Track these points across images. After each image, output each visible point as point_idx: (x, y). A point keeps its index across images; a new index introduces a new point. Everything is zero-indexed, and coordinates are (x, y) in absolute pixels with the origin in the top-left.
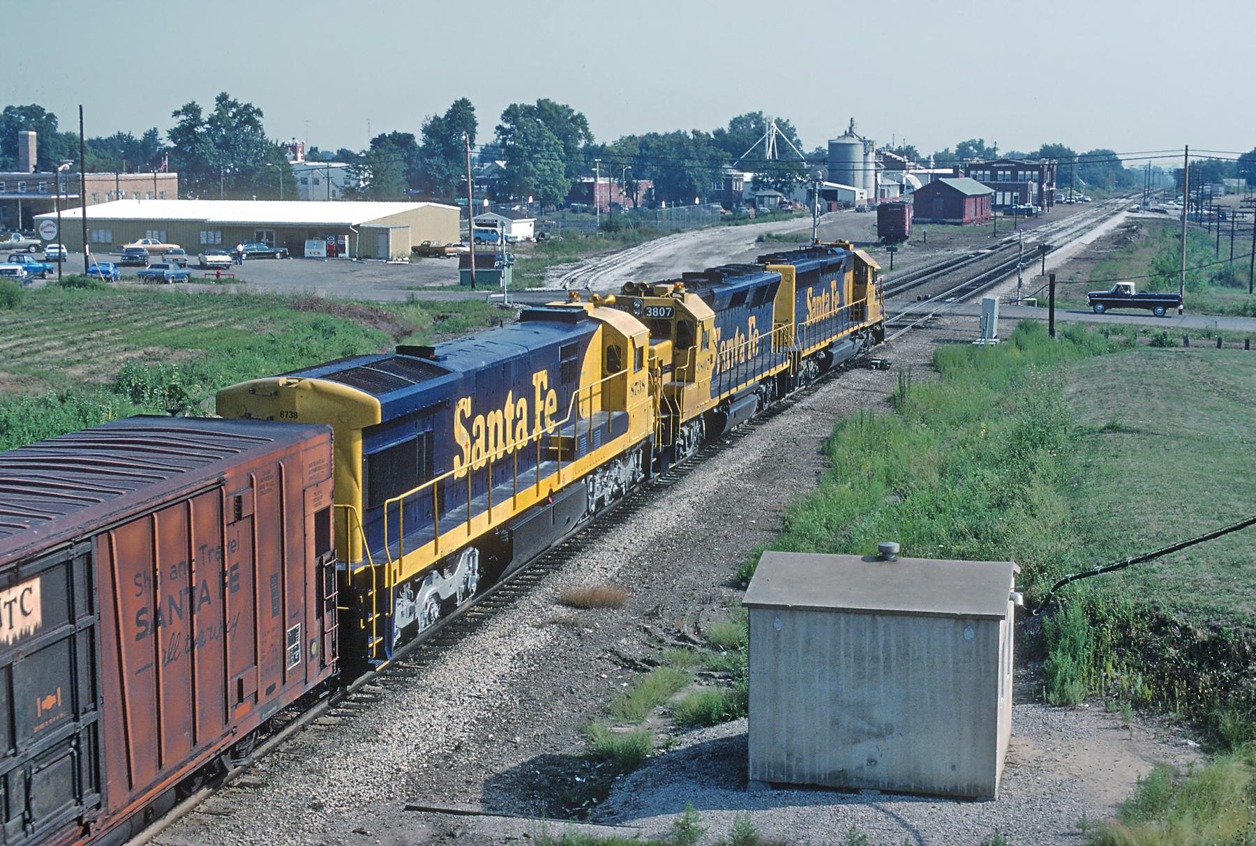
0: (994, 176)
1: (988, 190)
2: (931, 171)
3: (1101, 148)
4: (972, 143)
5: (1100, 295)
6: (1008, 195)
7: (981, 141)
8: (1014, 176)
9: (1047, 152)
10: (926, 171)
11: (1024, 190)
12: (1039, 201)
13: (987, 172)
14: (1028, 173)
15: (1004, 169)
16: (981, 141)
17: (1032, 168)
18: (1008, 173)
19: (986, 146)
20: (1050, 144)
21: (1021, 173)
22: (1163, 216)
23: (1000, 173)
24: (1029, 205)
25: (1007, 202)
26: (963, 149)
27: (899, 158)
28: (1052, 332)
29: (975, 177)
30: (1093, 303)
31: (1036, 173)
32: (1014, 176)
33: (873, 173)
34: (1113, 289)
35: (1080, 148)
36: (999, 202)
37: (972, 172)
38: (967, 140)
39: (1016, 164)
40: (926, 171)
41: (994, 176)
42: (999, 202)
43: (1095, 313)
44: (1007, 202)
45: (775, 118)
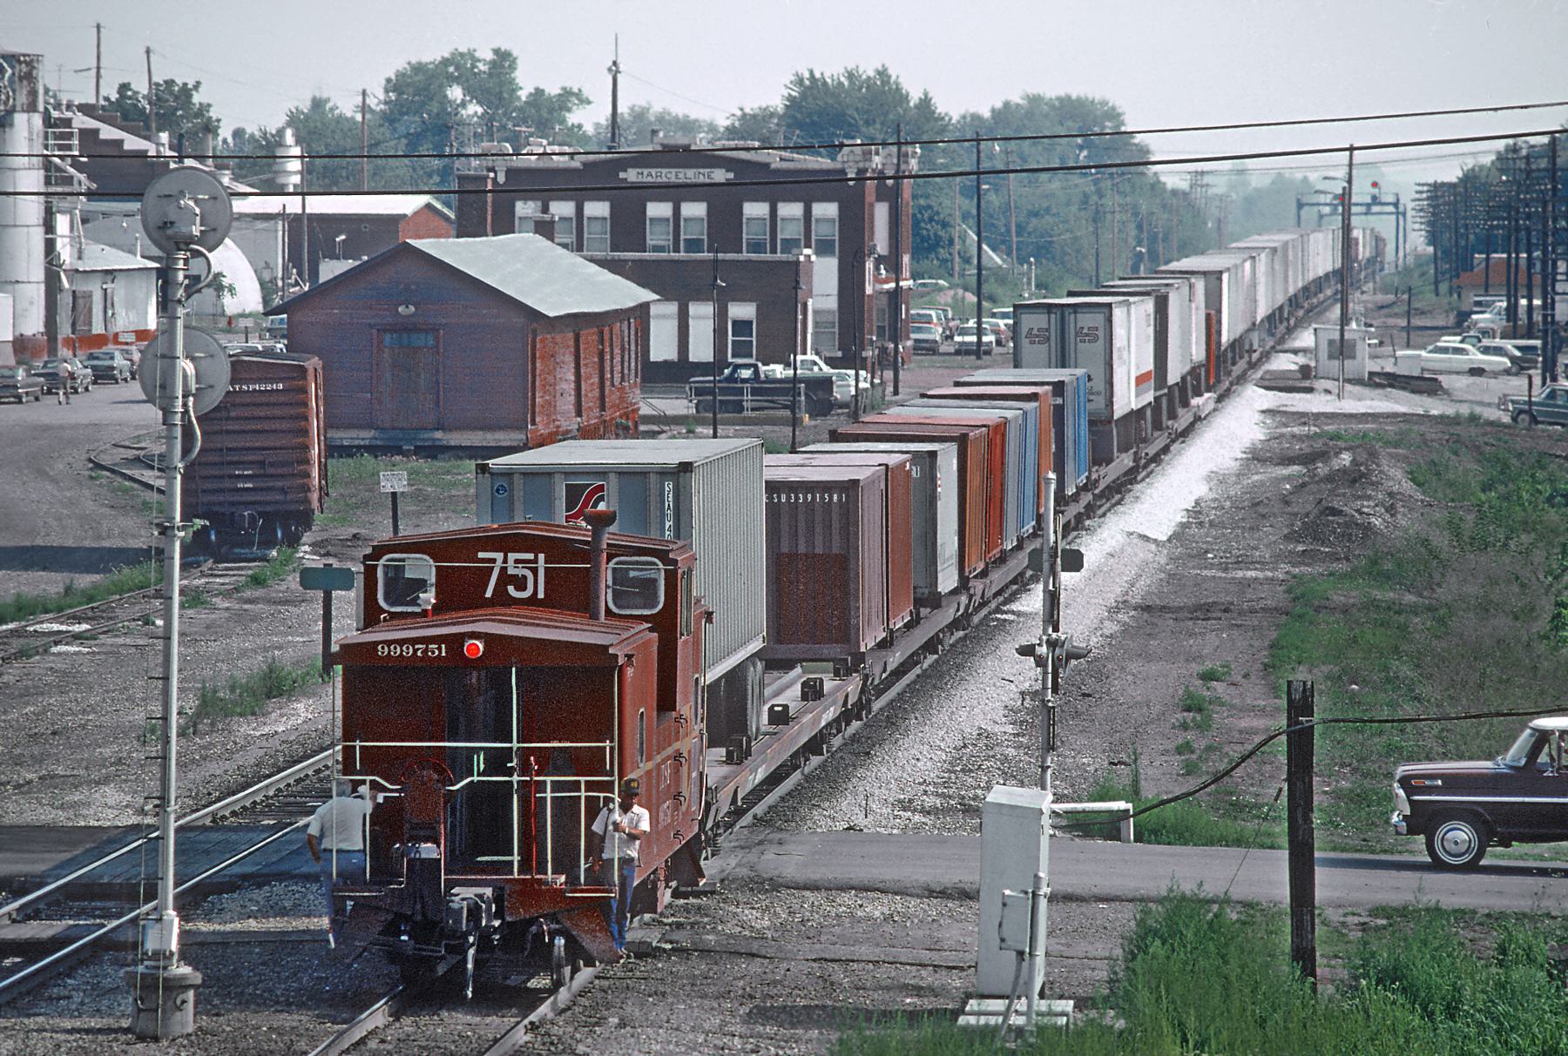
0: (628, 227)
1: (624, 293)
2: (293, 205)
3: (1052, 88)
4: (458, 67)
5: (1454, 783)
6: (702, 315)
7: (503, 61)
8: (725, 224)
9: (820, 112)
10: (272, 204)
11: (780, 287)
12: (852, 333)
13: (597, 209)
14: (791, 210)
15: (677, 193)
16: (503, 61)
17: (807, 187)
18: (695, 210)
19: (526, 81)
20: (832, 69)
21: (755, 210)
22: (1436, 407)
23: (658, 210)
24: (811, 362)
25: (701, 351)
26: (417, 91)
27: (132, 143)
28: (1304, 955)
29: (545, 228)
30: (1424, 821)
31: (827, 210)
32: (725, 224)
33: (31, 210)
34: (1516, 752)
35: (961, 83)
36: (662, 348)
37: (525, 209)
38: (432, 53)
39: (735, 173)
40: (272, 204)
41: (628, 227)
42: (662, 348)
43: (1438, 866)
44: (701, 351)
45: (842, 71)
